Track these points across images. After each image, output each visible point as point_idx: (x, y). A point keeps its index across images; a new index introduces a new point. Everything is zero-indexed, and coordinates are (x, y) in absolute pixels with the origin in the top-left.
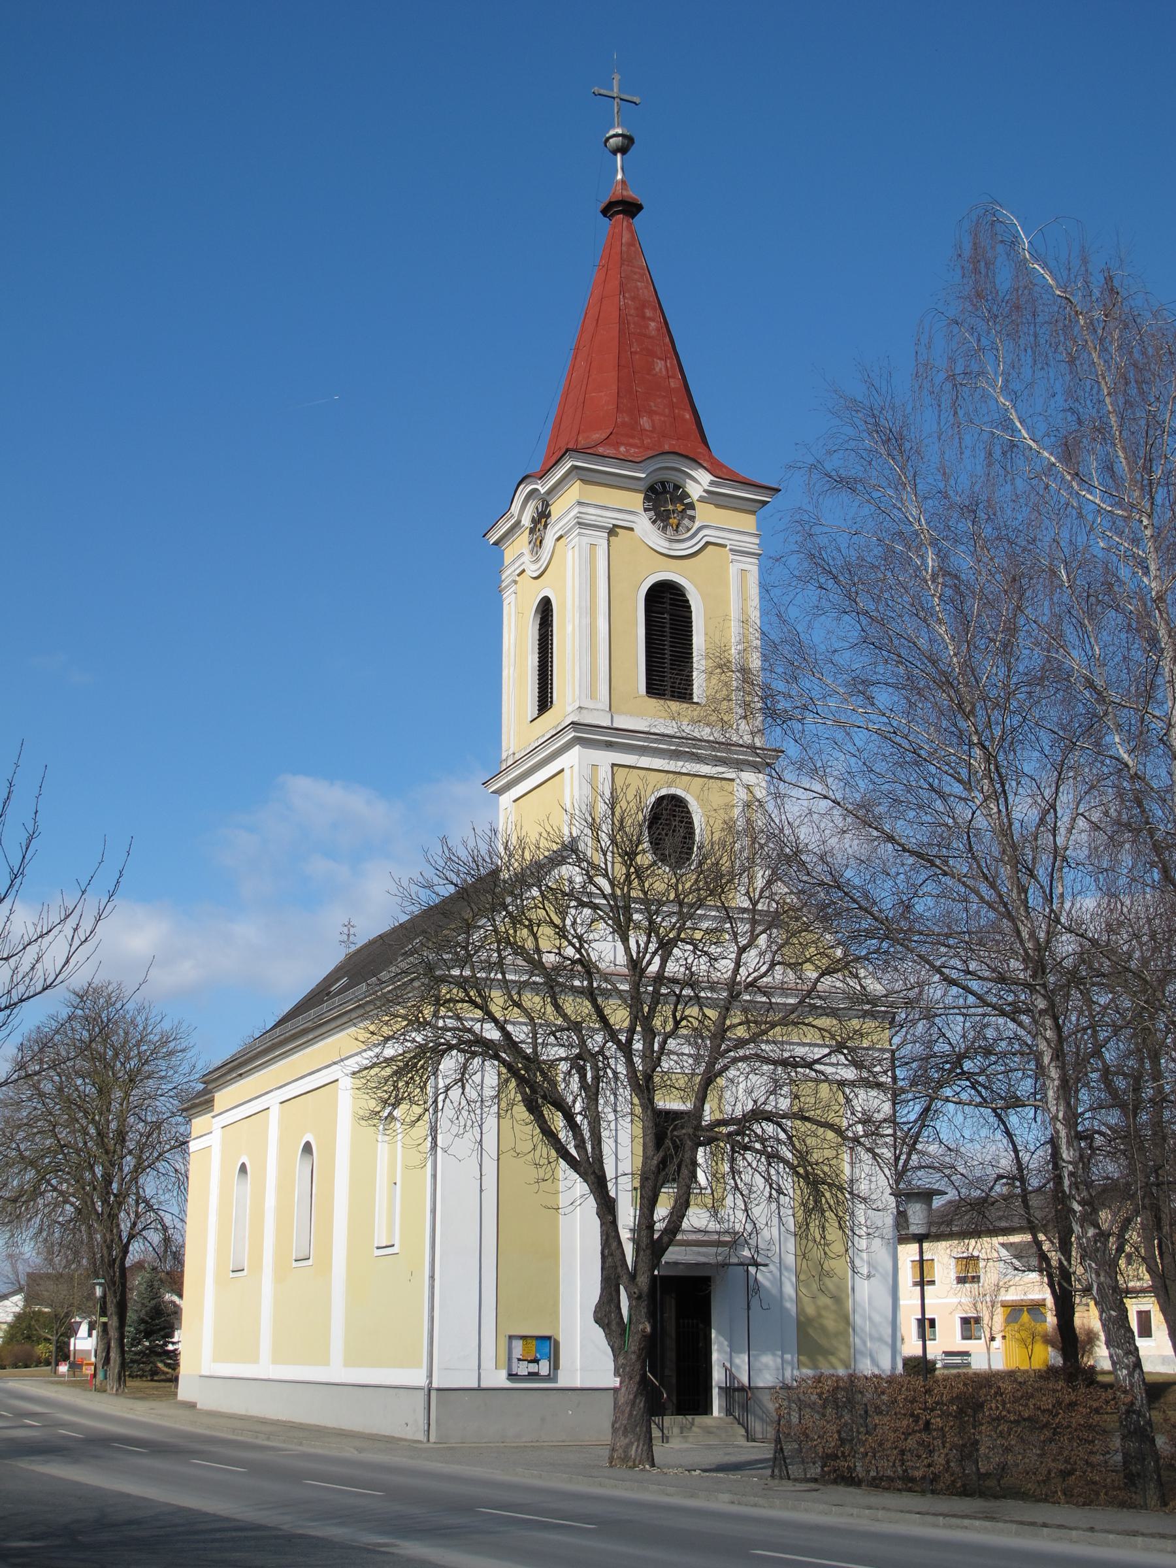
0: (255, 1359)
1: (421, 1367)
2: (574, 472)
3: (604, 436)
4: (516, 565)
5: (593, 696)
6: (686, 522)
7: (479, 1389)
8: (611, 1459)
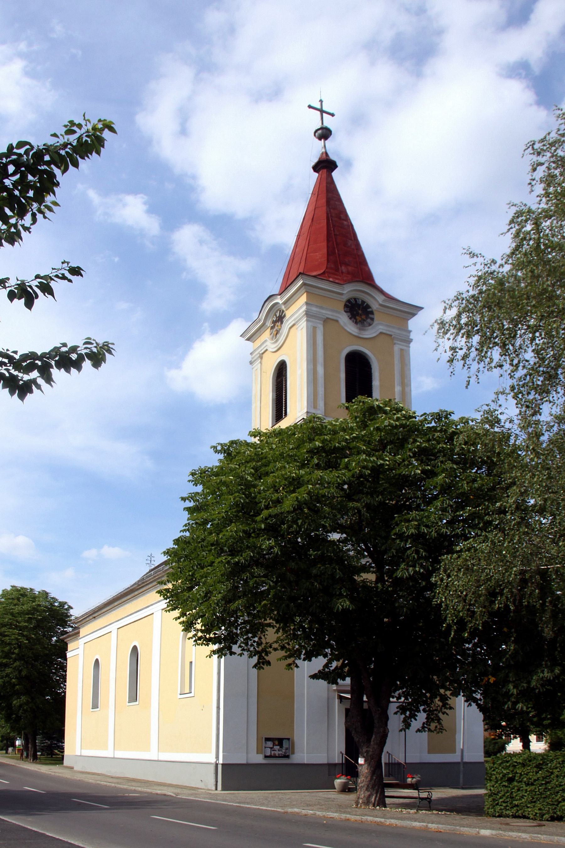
0: (148, 749)
1: (211, 753)
2: (303, 287)
3: (322, 271)
4: (262, 348)
5: (315, 407)
6: (369, 320)
7: (114, 758)
8: (357, 803)
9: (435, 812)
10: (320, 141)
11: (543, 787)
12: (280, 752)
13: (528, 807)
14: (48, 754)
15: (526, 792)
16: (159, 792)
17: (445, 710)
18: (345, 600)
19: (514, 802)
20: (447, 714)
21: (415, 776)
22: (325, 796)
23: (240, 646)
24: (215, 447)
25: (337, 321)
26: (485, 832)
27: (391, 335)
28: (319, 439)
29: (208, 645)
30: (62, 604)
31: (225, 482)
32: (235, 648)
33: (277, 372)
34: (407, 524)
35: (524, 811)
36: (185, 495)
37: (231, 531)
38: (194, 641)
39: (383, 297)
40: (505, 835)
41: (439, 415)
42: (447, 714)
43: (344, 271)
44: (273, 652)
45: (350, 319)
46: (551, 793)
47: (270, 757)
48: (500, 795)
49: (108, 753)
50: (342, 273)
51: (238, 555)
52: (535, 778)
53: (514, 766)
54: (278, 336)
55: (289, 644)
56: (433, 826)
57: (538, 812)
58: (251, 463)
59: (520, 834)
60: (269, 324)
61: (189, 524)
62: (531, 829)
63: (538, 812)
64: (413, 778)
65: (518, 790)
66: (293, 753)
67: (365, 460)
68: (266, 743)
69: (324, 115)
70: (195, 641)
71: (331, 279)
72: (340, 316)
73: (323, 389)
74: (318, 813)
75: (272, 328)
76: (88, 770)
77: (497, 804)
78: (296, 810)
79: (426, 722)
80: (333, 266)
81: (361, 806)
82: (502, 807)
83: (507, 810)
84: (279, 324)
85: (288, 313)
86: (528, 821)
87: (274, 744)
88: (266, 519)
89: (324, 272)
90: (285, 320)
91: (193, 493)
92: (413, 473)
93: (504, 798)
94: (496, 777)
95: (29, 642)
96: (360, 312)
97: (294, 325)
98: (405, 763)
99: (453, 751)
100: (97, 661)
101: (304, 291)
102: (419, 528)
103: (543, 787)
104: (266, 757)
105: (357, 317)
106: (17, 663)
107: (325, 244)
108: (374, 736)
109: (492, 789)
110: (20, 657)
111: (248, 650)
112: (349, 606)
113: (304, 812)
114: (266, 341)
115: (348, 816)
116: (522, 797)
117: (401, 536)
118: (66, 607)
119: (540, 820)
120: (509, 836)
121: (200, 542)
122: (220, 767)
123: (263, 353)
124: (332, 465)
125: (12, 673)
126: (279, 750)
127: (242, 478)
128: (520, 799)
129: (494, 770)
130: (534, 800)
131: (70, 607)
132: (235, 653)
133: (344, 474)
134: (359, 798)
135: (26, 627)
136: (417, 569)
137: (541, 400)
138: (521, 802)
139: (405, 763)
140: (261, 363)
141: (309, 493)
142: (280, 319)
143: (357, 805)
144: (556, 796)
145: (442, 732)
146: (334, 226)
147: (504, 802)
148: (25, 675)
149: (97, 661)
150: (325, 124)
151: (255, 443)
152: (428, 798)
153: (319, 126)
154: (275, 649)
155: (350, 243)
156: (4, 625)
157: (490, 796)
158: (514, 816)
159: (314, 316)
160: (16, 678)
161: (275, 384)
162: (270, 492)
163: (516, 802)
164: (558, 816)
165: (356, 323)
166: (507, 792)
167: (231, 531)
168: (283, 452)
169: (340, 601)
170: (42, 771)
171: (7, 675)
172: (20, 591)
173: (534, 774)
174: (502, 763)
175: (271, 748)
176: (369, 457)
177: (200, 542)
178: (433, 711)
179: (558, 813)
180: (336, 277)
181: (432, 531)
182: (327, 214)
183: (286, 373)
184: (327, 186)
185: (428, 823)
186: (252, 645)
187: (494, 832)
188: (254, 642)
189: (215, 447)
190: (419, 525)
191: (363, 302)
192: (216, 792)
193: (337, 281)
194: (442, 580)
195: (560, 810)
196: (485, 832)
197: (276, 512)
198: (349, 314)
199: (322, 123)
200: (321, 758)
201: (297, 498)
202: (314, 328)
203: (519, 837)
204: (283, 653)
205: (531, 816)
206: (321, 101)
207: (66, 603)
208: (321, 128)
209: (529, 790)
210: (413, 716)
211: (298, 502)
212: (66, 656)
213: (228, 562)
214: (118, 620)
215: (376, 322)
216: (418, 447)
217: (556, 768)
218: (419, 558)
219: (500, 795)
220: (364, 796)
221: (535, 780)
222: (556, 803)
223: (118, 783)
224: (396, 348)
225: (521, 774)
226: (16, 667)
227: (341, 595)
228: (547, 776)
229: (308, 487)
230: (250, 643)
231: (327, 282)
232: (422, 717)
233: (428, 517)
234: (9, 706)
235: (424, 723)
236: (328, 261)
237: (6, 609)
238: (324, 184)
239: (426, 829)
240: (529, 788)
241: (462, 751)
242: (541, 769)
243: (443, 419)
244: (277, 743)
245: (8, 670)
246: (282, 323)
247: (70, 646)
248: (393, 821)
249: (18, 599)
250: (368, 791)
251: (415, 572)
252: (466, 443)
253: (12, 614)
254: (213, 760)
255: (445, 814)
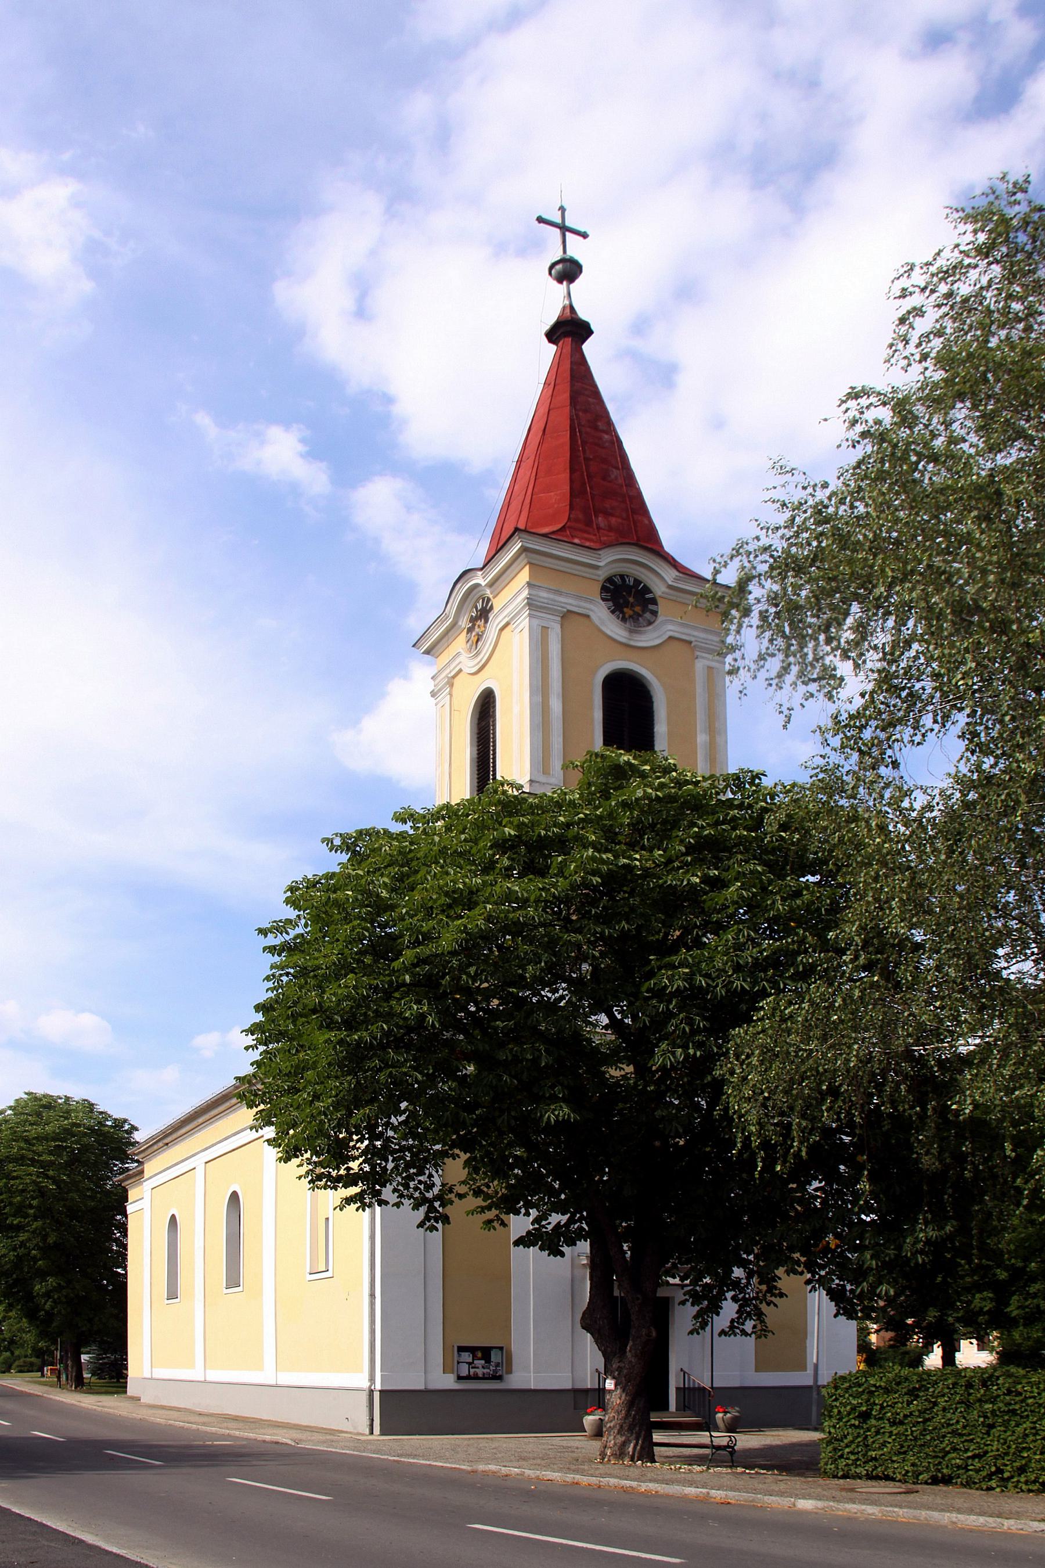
0: (259, 1367)
2: (523, 555)
3: (560, 526)
4: (452, 667)
5: (546, 771)
6: (648, 615)
7: (205, 1381)
8: (603, 1455)
9: (740, 1470)
10: (559, 285)
11: (920, 1427)
12: (485, 1371)
13: (893, 1462)
14: (112, 1378)
15: (890, 1437)
16: (268, 1438)
17: (773, 1299)
18: (561, 1107)
19: (870, 1453)
20: (776, 1305)
21: (730, 1410)
22: (565, 1444)
23: (395, 1190)
24: (328, 841)
25: (588, 616)
26: (806, 1504)
27: (690, 642)
28: (511, 823)
29: (335, 1188)
30: (119, 1123)
31: (336, 901)
32: (387, 1193)
33: (478, 710)
34: (670, 973)
35: (887, 1468)
36: (266, 925)
37: (346, 987)
38: (309, 1182)
39: (674, 573)
40: (838, 1509)
41: (738, 778)
42: (776, 1305)
43: (602, 525)
44: (456, 1200)
45: (613, 612)
46: (932, 1438)
47: (468, 1378)
48: (846, 1441)
49: (195, 1373)
50: (599, 528)
51: (357, 1030)
52: (907, 1412)
53: (871, 1393)
54: (480, 644)
55: (489, 1187)
56: (717, 1494)
57: (910, 1469)
58: (390, 869)
59: (864, 1507)
60: (464, 622)
61: (273, 975)
62: (889, 1498)
63: (910, 1469)
64: (726, 1412)
65: (877, 1433)
66: (510, 1371)
67: (593, 859)
68: (459, 1355)
69: (568, 234)
70: (311, 1182)
71: (576, 541)
72: (592, 607)
73: (561, 740)
74: (528, 1472)
75: (470, 630)
76: (164, 1403)
77: (841, 1457)
78: (492, 1467)
79: (738, 1318)
80: (581, 516)
81: (609, 1460)
82: (850, 1462)
83: (857, 1466)
84: (481, 623)
85: (497, 603)
86: (892, 1484)
87: (475, 1357)
88: (415, 965)
89: (564, 527)
90: (491, 616)
91: (280, 921)
92: (685, 883)
93: (853, 1446)
94: (839, 1412)
95: (59, 1187)
96: (631, 600)
97: (507, 624)
98: (712, 1388)
99: (804, 1368)
100: (173, 1217)
101: (525, 561)
102: (692, 979)
103: (920, 1427)
104: (460, 1378)
105: (625, 610)
106: (38, 1224)
107: (565, 476)
108: (631, 1343)
109: (833, 1430)
110: (43, 1213)
111: (410, 1197)
112: (569, 1115)
113: (504, 1470)
114: (458, 654)
115: (578, 1477)
116: (884, 1444)
117: (659, 993)
118: (127, 1127)
119: (914, 1483)
120: (845, 1510)
121: (290, 1007)
122: (377, 1396)
123: (454, 677)
124: (533, 868)
125: (29, 1240)
126: (483, 1367)
127: (370, 893)
128: (880, 1448)
129: (836, 1400)
130: (904, 1449)
131: (134, 1128)
132: (386, 1203)
133: (554, 885)
134: (605, 1447)
135: (52, 1163)
136: (691, 1051)
137: (888, 739)
138: (881, 1452)
139: (712, 1388)
140: (451, 694)
141: (489, 919)
142: (484, 614)
143: (603, 1459)
144: (941, 1442)
145: (766, 1336)
146: (584, 443)
147: (852, 1453)
148: (55, 1242)
149: (173, 1217)
150: (571, 253)
151: (407, 832)
152: (728, 1446)
153: (558, 255)
154: (461, 1196)
155: (614, 473)
156: (9, 1159)
157: (829, 1443)
158: (870, 1477)
159: (545, 608)
160: (39, 1249)
161: (476, 731)
162: (419, 917)
163: (873, 1454)
164: (943, 1475)
165: (624, 620)
166: (858, 1436)
167: (346, 987)
168: (445, 847)
169: (553, 1107)
170: (83, 1405)
171: (23, 1244)
172: (41, 1100)
173: (905, 1405)
174: (850, 1387)
175: (469, 1364)
176: (599, 852)
177: (290, 1007)
178: (751, 1299)
179: (945, 1471)
180: (586, 535)
181: (717, 985)
182: (572, 420)
183: (494, 711)
184: (572, 370)
185: (712, 1489)
186: (416, 1189)
187: (820, 1504)
188: (420, 1182)
189: (328, 841)
190: (692, 974)
191: (637, 582)
192: (371, 1437)
193: (587, 544)
194: (732, 1072)
195: (947, 1467)
196: (806, 1504)
197: (428, 952)
198: (611, 604)
199: (565, 252)
200: (560, 1380)
201: (465, 927)
202: (545, 629)
203: (862, 1512)
204: (479, 1202)
205: (899, 1477)
206: (562, 209)
207: (125, 1121)
208: (562, 261)
209: (895, 1432)
210: (715, 1308)
211: (467, 934)
212: (126, 1211)
213: (341, 1042)
214: (206, 1149)
215: (661, 618)
216: (697, 836)
217: (943, 1396)
218: (694, 1032)
219: (846, 1441)
220: (615, 1444)
221: (906, 1416)
222: (940, 1455)
223: (204, 1424)
224: (700, 665)
225: (881, 1405)
226: (36, 1229)
227: (554, 1099)
228: (926, 1409)
229: (485, 908)
230: (412, 1184)
231: (567, 546)
232: (729, 1309)
233: (711, 959)
234: (29, 1297)
235: (732, 1321)
236: (572, 507)
237: (15, 1132)
238: (567, 366)
239: (705, 1500)
240: (895, 1430)
241: (816, 1366)
242: (917, 1397)
243: (747, 786)
244: (479, 1355)
245: (23, 1237)
246: (486, 621)
247: (132, 1194)
248: (652, 1486)
249: (39, 1114)
250: (624, 1435)
251: (687, 1056)
252: (783, 827)
253: (27, 1141)
254: (365, 1384)
255: (757, 1473)
